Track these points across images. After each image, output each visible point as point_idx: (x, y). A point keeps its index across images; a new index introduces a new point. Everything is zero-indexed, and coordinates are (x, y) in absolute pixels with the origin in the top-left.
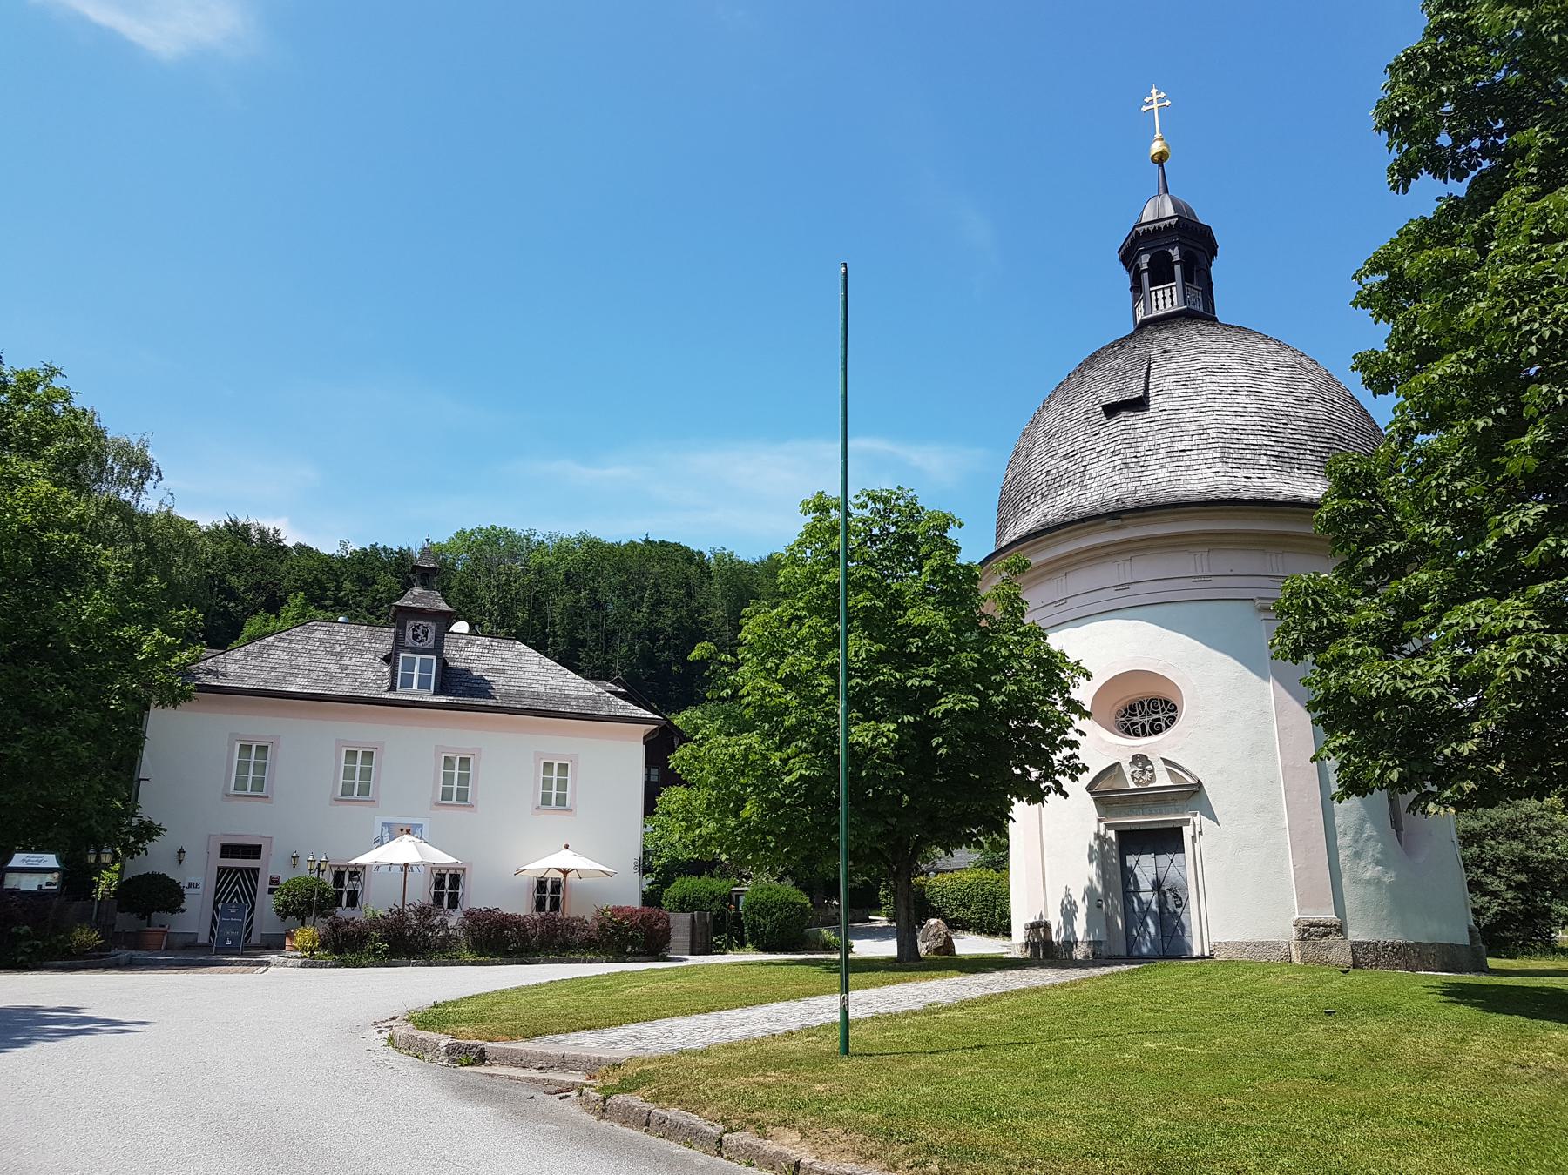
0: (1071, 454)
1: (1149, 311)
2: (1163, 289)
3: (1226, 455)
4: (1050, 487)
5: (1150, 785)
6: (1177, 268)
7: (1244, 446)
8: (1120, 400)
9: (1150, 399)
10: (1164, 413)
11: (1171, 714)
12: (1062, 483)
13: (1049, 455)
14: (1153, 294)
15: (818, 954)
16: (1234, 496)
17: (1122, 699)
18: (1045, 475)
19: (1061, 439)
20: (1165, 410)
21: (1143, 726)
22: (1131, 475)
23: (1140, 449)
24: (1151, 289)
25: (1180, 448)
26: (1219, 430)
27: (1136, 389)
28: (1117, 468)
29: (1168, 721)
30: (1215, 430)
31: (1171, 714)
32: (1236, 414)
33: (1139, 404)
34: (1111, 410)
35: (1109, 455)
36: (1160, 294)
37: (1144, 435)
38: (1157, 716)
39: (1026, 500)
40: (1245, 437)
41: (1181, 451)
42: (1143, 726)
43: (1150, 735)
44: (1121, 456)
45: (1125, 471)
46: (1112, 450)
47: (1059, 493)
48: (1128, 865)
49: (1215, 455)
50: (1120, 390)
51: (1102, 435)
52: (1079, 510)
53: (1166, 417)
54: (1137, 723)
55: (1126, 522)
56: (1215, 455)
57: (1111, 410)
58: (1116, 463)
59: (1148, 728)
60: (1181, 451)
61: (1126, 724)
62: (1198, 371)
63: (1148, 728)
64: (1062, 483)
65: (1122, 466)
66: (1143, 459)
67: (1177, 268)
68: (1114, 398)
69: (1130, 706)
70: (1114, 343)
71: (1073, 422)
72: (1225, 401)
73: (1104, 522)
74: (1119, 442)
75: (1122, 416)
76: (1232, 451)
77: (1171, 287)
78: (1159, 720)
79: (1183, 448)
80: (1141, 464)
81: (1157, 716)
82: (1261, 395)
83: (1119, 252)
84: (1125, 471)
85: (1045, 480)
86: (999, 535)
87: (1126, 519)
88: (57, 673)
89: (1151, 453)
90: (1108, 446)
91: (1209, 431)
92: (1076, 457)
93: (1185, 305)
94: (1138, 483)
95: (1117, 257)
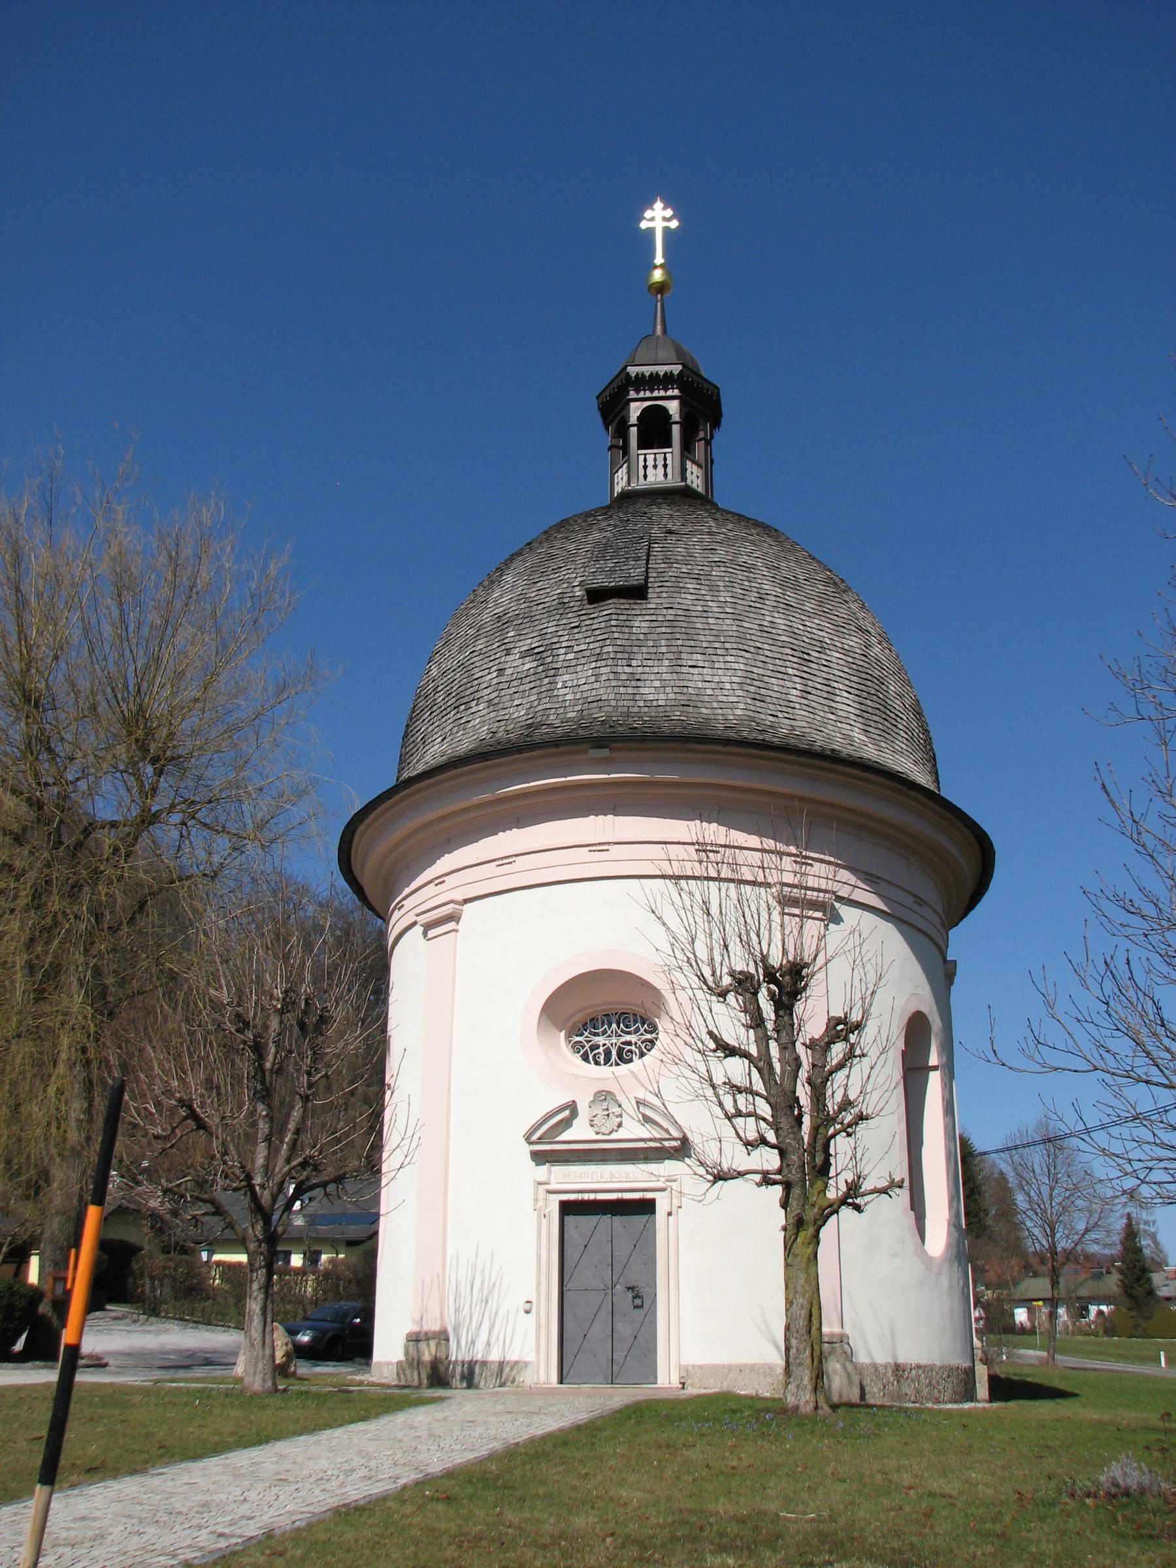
0: (536, 651)
1: (633, 480)
2: (655, 454)
3: (748, 681)
4: (503, 693)
5: (614, 1136)
6: (676, 430)
7: (769, 673)
8: (613, 584)
9: (650, 590)
10: (670, 611)
11: (649, 1036)
12: (521, 688)
13: (503, 647)
14: (641, 458)
15: (104, 1385)
16: (760, 737)
17: (579, 1011)
18: (495, 674)
19: (522, 626)
20: (671, 608)
21: (608, 1054)
22: (622, 690)
23: (636, 656)
24: (640, 452)
25: (690, 663)
26: (741, 646)
27: (635, 575)
28: (604, 677)
29: (643, 1047)
30: (735, 646)
31: (649, 1036)
32: (762, 628)
33: (638, 593)
34: (596, 596)
35: (593, 659)
36: (650, 458)
37: (642, 637)
38: (628, 1038)
39: (463, 707)
40: (772, 661)
41: (690, 666)
42: (608, 1054)
43: (617, 1064)
44: (610, 662)
45: (614, 683)
46: (598, 651)
47: (516, 703)
48: (1017, 1322)
49: (734, 679)
50: (613, 571)
51: (584, 629)
52: (544, 730)
53: (671, 618)
54: (598, 1047)
55: (616, 754)
56: (734, 679)
57: (596, 596)
58: (603, 670)
59: (614, 1053)
60: (690, 666)
61: (583, 1047)
62: (713, 564)
63: (614, 1053)
64: (521, 688)
65: (612, 676)
66: (640, 670)
67: (676, 430)
68: (603, 581)
69: (591, 1020)
70: (596, 510)
71: (541, 606)
72: (747, 609)
73: (585, 751)
74: (608, 642)
75: (611, 606)
76: (755, 676)
77: (665, 454)
78: (629, 1043)
79: (694, 663)
80: (637, 677)
81: (628, 1038)
82: (791, 608)
83: (598, 397)
84: (614, 683)
85: (495, 681)
86: (403, 761)
87: (617, 749)
88: (931, 1410)
89: (650, 663)
90: (592, 646)
91: (727, 645)
92: (545, 655)
93: (682, 481)
94: (631, 703)
95: (595, 404)
